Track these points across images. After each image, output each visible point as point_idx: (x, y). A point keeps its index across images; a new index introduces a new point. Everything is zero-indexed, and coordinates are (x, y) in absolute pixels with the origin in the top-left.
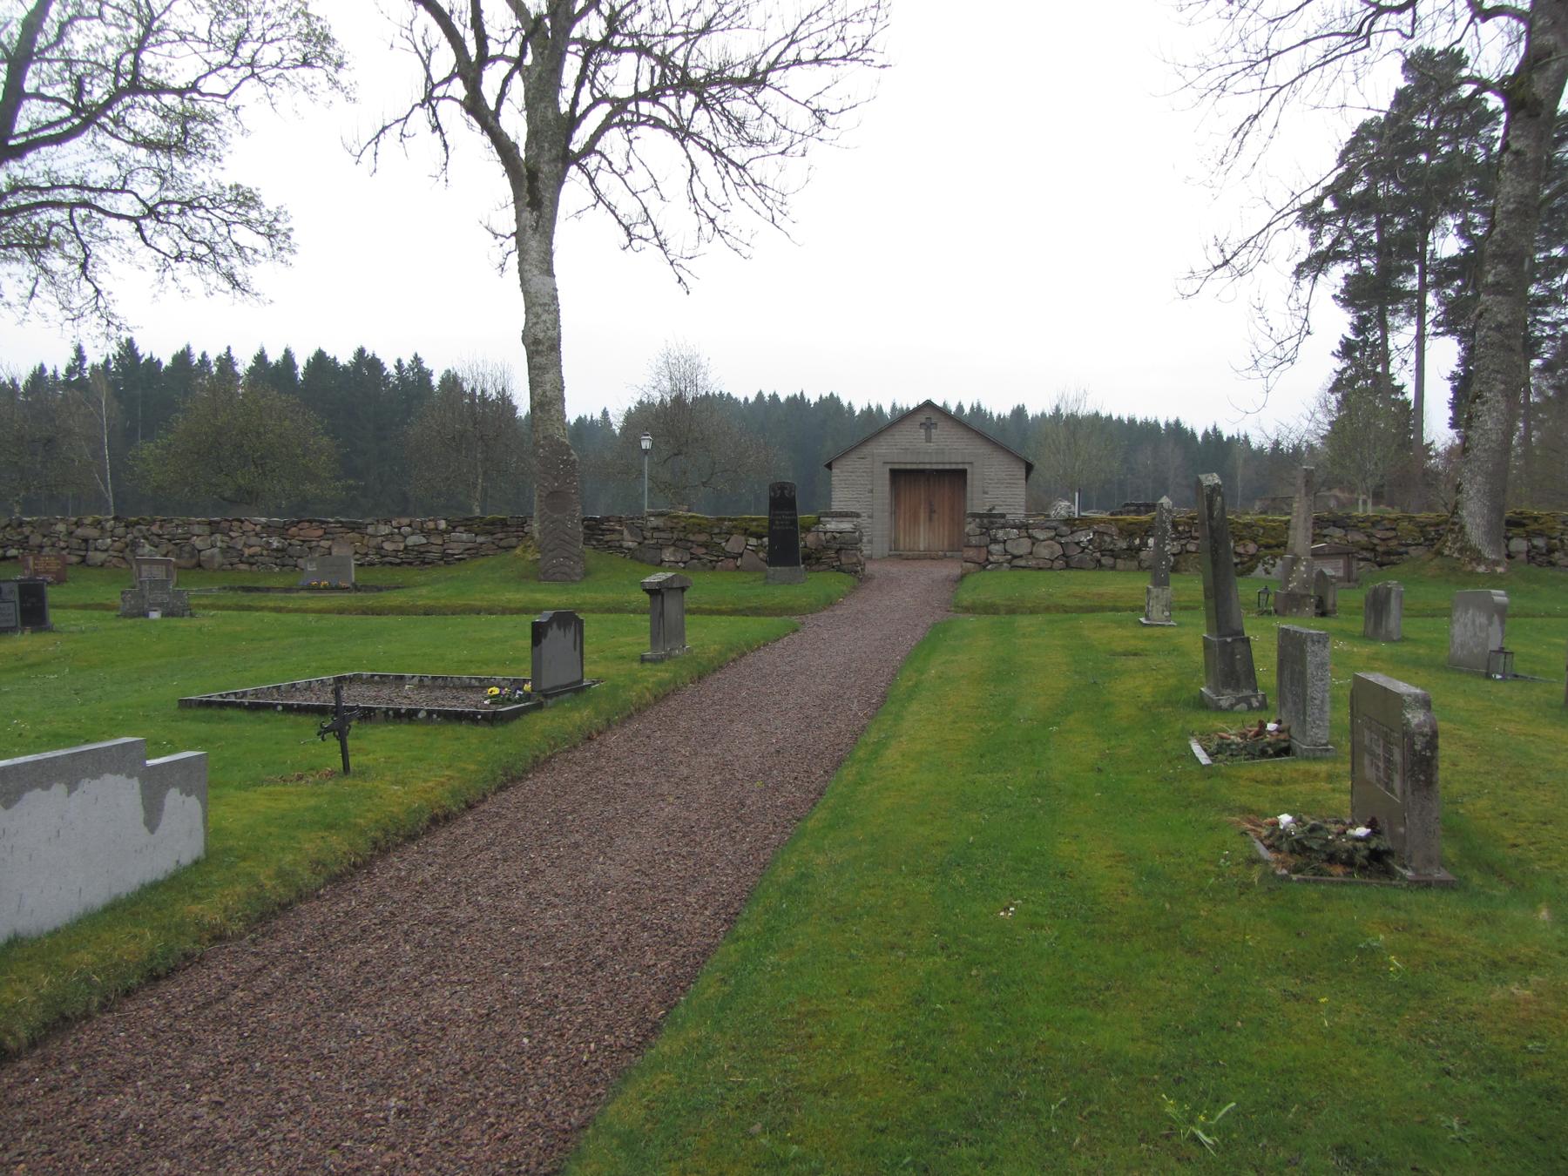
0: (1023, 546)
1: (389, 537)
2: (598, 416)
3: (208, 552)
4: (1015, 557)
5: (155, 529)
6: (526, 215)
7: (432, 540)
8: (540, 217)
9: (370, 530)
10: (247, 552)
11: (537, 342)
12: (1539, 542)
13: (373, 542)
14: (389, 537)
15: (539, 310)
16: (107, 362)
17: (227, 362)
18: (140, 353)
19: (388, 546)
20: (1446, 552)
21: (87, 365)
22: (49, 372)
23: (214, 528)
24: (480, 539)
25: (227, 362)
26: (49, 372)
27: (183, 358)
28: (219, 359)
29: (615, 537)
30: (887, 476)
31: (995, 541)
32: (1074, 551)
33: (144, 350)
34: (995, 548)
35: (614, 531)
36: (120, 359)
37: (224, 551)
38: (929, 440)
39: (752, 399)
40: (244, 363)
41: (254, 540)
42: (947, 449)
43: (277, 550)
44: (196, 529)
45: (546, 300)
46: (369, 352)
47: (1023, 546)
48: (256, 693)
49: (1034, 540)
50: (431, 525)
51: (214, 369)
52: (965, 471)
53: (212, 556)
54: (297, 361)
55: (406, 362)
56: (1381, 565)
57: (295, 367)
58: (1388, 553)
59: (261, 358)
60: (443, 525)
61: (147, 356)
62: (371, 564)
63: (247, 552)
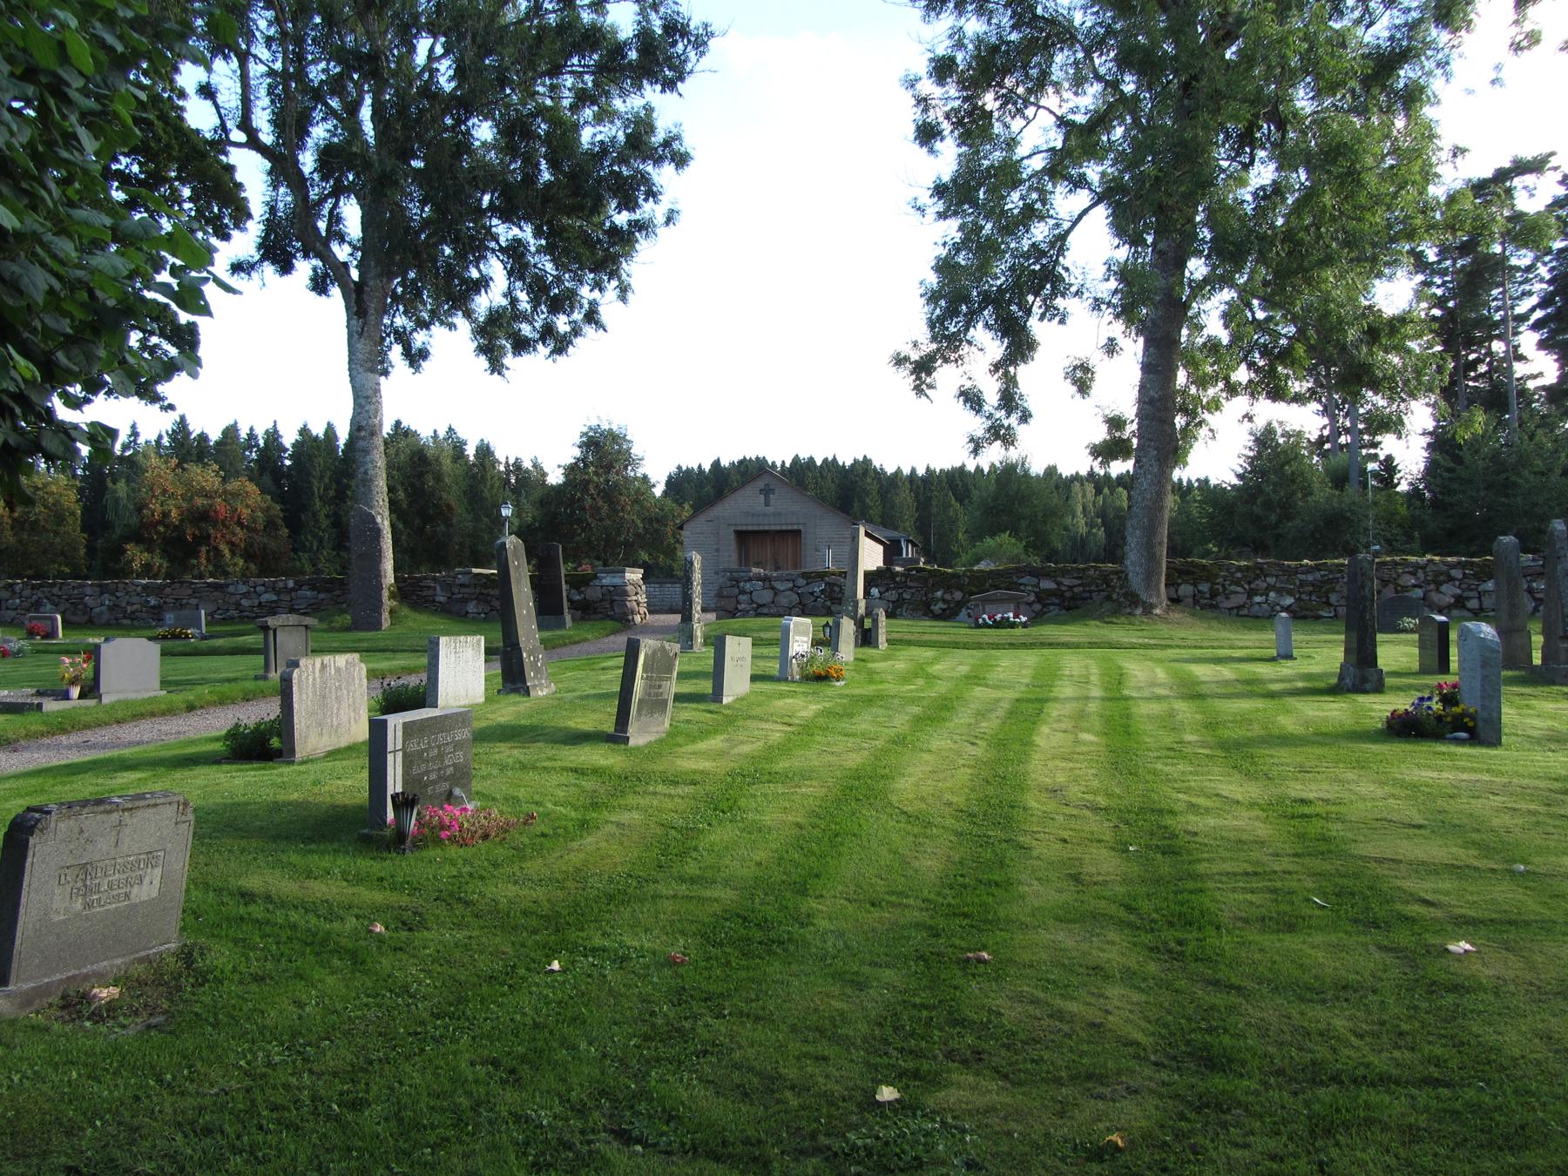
0: (766, 596)
1: (246, 595)
2: (1428, 439)
3: (97, 610)
4: (760, 606)
5: (55, 590)
6: (354, 322)
7: (283, 597)
8: (364, 324)
9: (231, 589)
10: (129, 609)
11: (360, 428)
12: (1204, 587)
13: (233, 599)
14: (246, 595)
15: (363, 401)
16: (160, 437)
17: (273, 436)
18: (191, 428)
19: (245, 602)
20: (1115, 596)
21: (141, 440)
22: (243, 434)
23: (103, 590)
24: (321, 596)
25: (273, 436)
26: (243, 434)
27: (230, 432)
28: (267, 432)
29: (430, 592)
30: (733, 536)
31: (743, 592)
32: (809, 601)
33: (195, 428)
34: (741, 597)
35: (429, 588)
36: (173, 435)
37: (110, 609)
38: (767, 504)
39: (707, 467)
40: (289, 438)
41: (135, 599)
42: (786, 509)
43: (153, 607)
44: (88, 591)
45: (370, 392)
46: (404, 424)
47: (766, 596)
48: (1435, 892)
49: (776, 592)
50: (281, 585)
51: (261, 443)
52: (797, 534)
53: (101, 613)
54: (339, 433)
55: (442, 434)
56: (1068, 609)
57: (337, 439)
58: (1073, 598)
59: (304, 431)
60: (291, 584)
61: (198, 432)
62: (232, 618)
63: (129, 609)
